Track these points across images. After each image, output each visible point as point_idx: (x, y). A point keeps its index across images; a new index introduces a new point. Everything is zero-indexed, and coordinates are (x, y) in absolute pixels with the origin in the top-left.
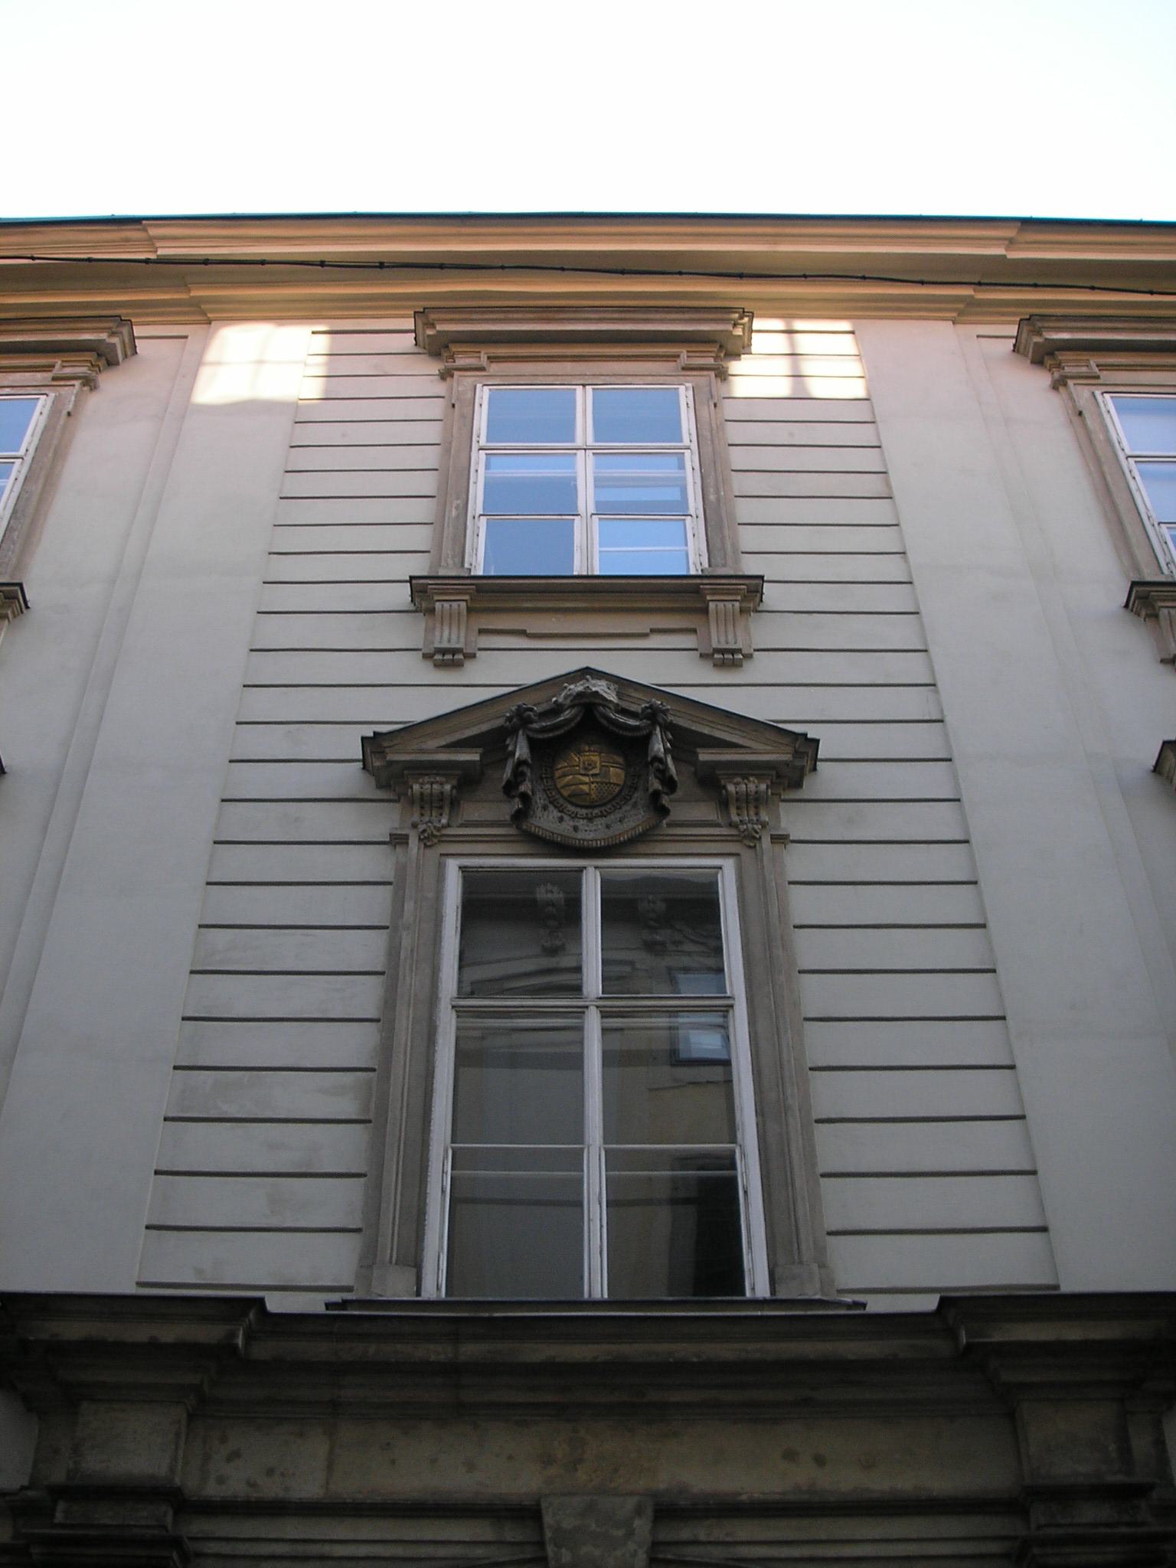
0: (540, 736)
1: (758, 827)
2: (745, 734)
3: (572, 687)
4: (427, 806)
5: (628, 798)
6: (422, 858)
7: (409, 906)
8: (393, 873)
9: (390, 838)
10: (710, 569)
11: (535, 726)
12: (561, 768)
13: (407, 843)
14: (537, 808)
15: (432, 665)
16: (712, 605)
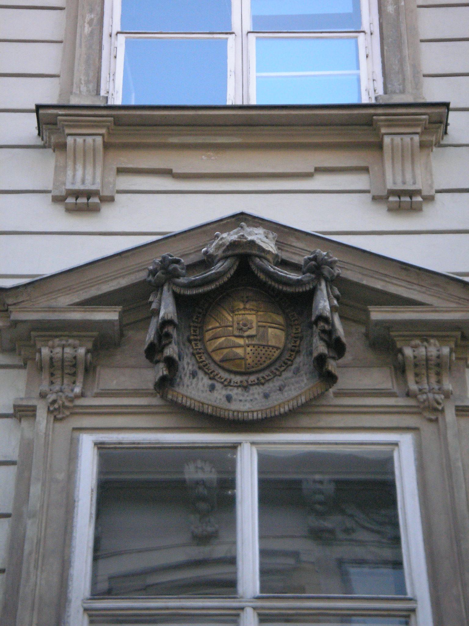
0: (189, 292)
1: (440, 397)
2: (424, 289)
3: (225, 235)
4: (58, 373)
5: (278, 373)
6: (51, 433)
7: (35, 490)
8: (17, 451)
9: (15, 410)
10: (387, 96)
11: (182, 280)
12: (212, 329)
13: (34, 416)
14: (185, 375)
15: (64, 210)
16: (387, 140)
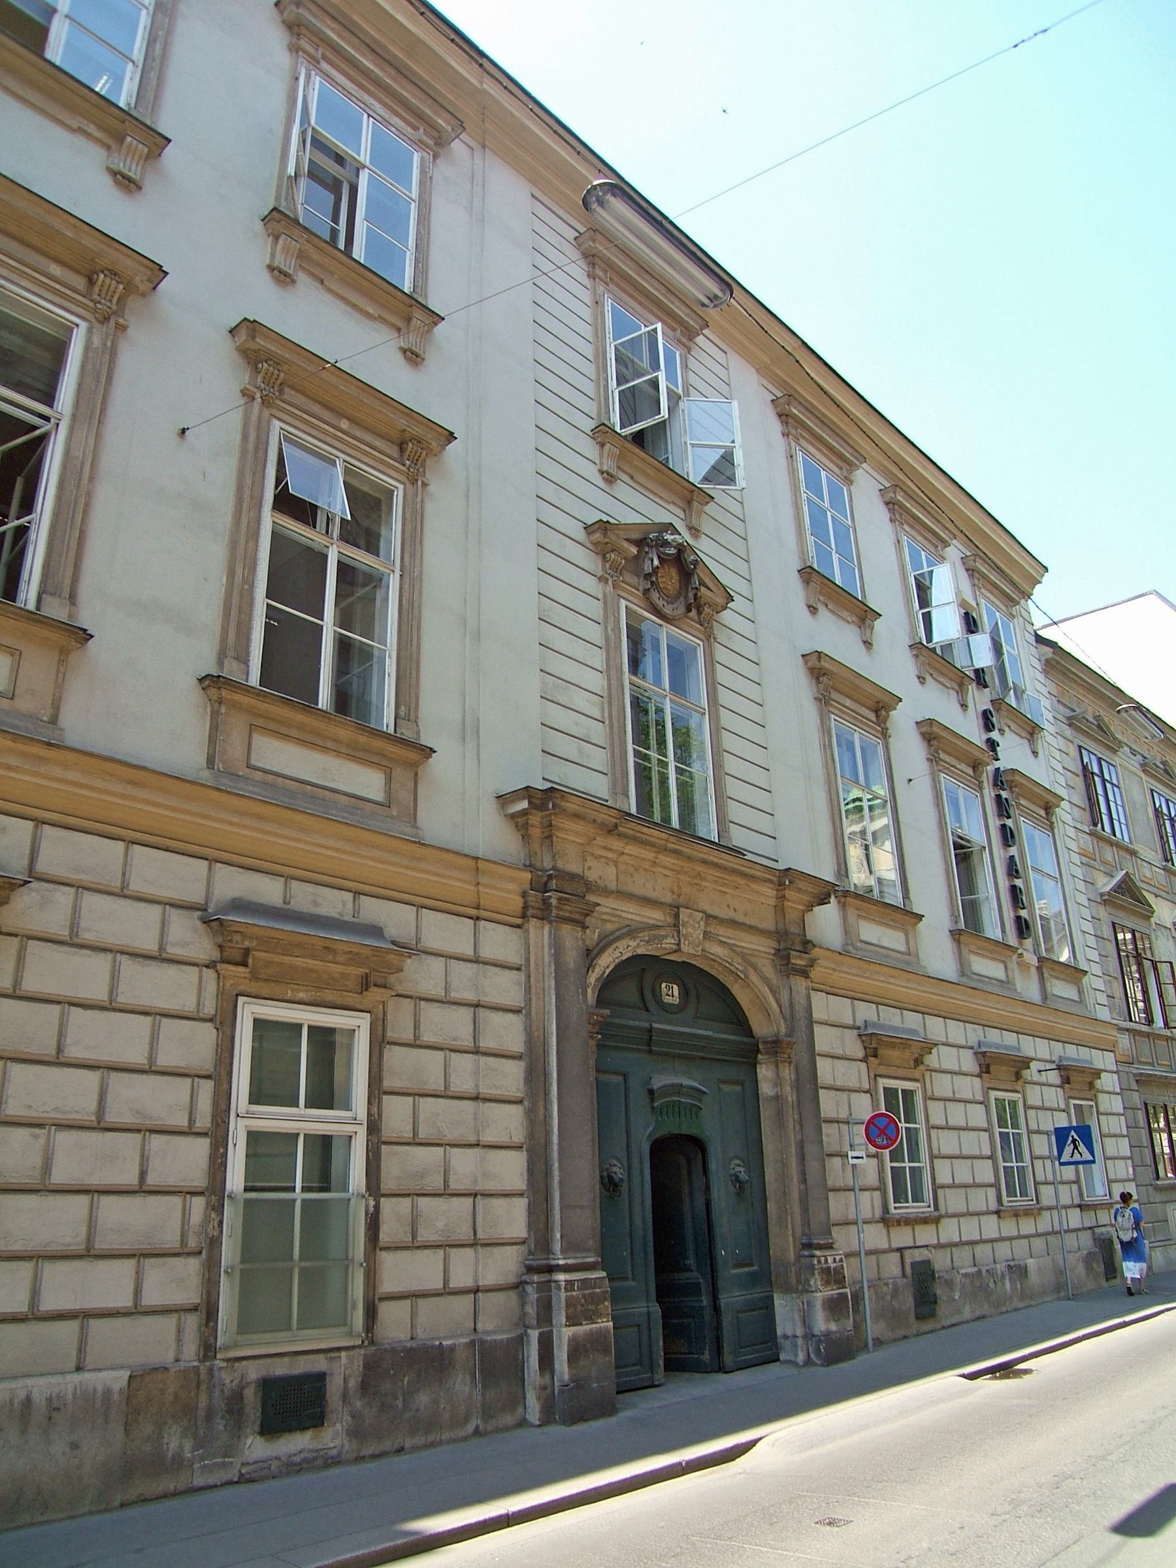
16: (129, 139)
